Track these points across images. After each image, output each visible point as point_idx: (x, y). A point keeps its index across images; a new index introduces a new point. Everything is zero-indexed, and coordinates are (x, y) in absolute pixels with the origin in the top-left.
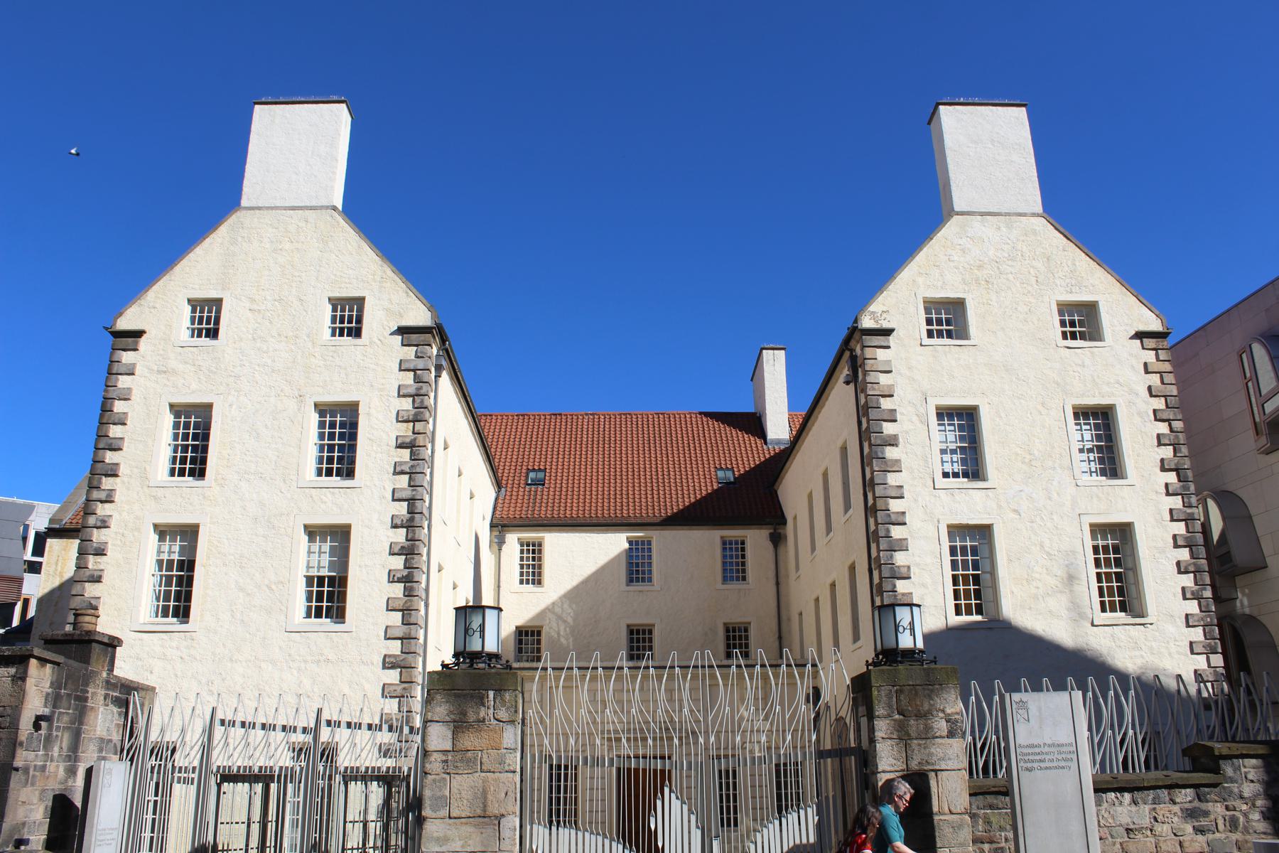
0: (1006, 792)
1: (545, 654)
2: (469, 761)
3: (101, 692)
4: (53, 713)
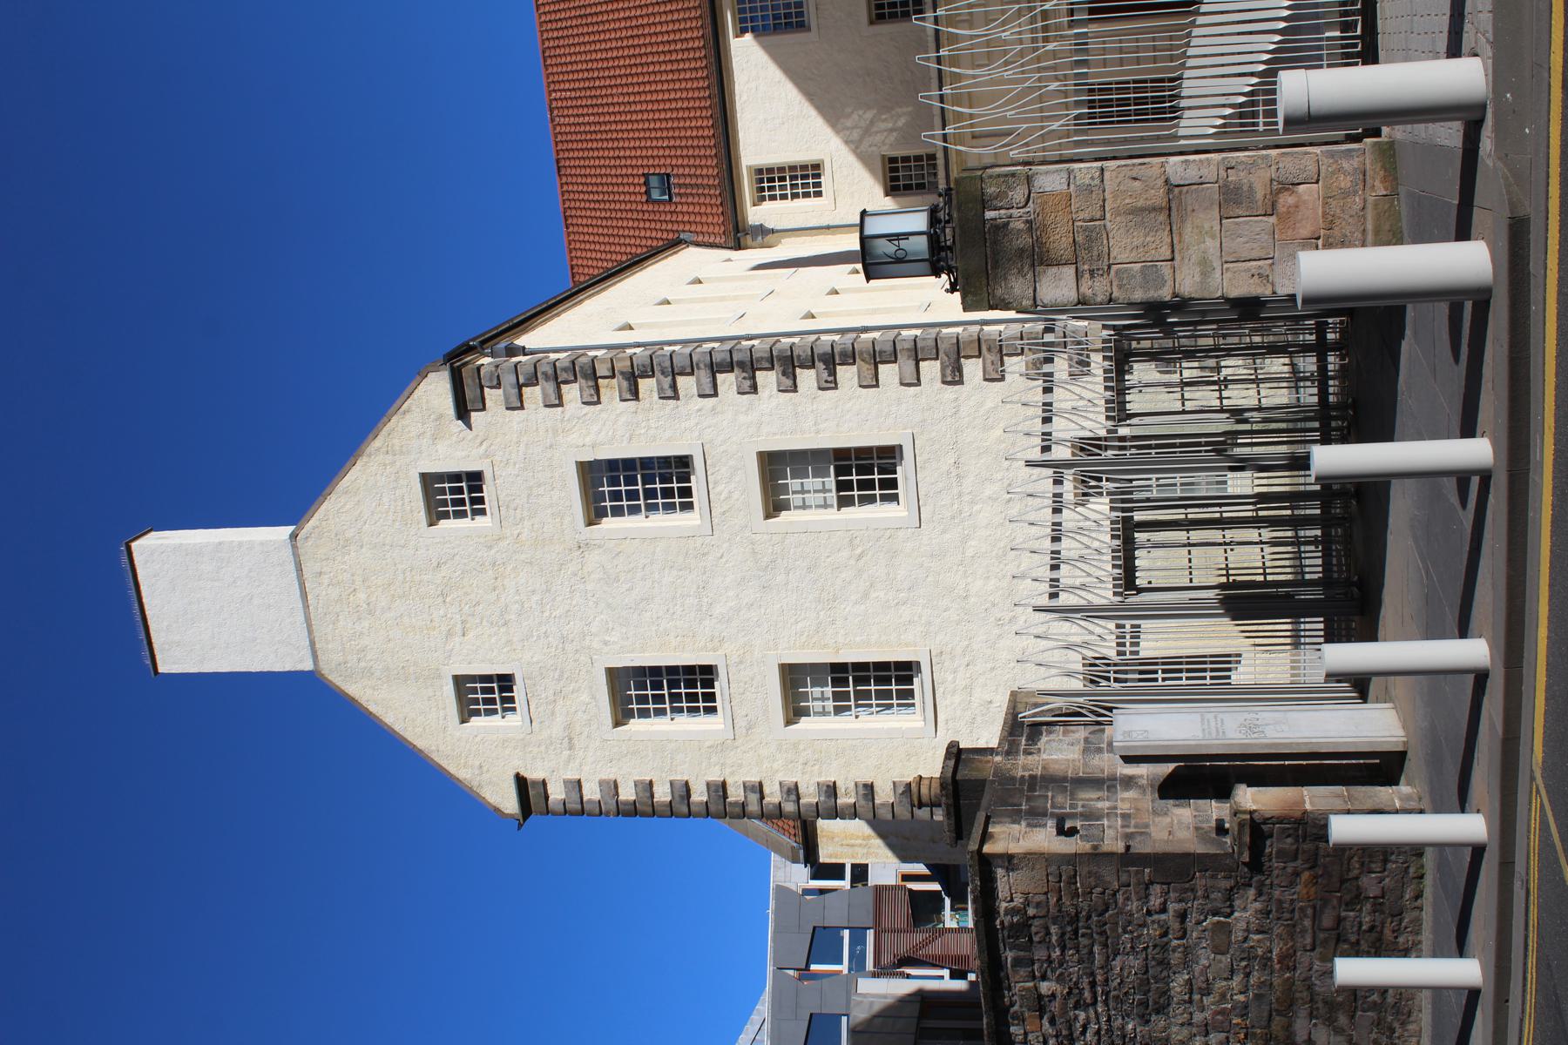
2: (1089, 239)
3: (1022, 759)
4: (1053, 815)
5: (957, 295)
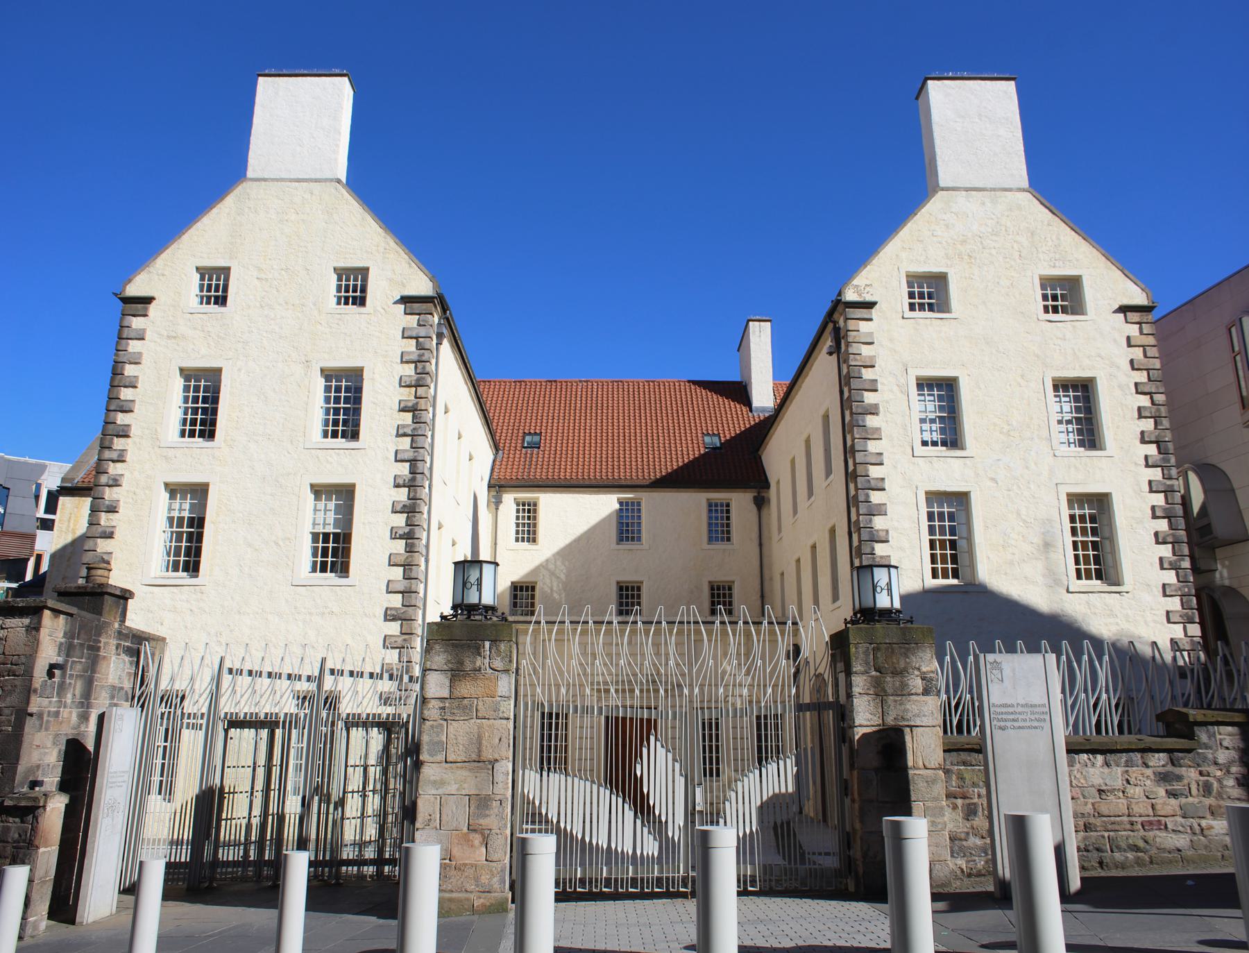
0: (980, 749)
1: (539, 607)
2: (465, 707)
3: (114, 642)
4: (67, 661)
5: (439, 620)
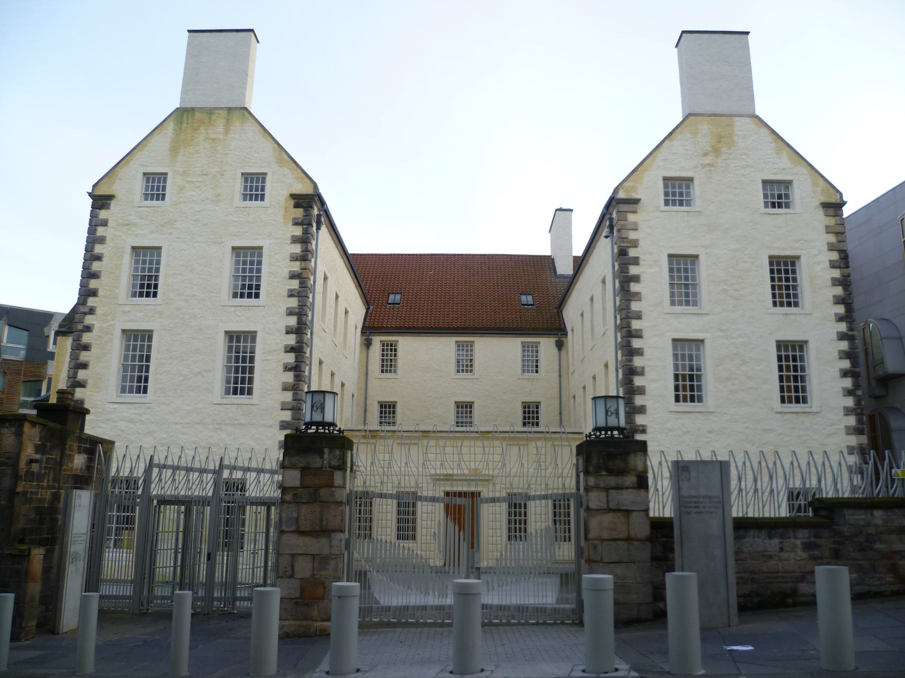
3: (75, 445)
